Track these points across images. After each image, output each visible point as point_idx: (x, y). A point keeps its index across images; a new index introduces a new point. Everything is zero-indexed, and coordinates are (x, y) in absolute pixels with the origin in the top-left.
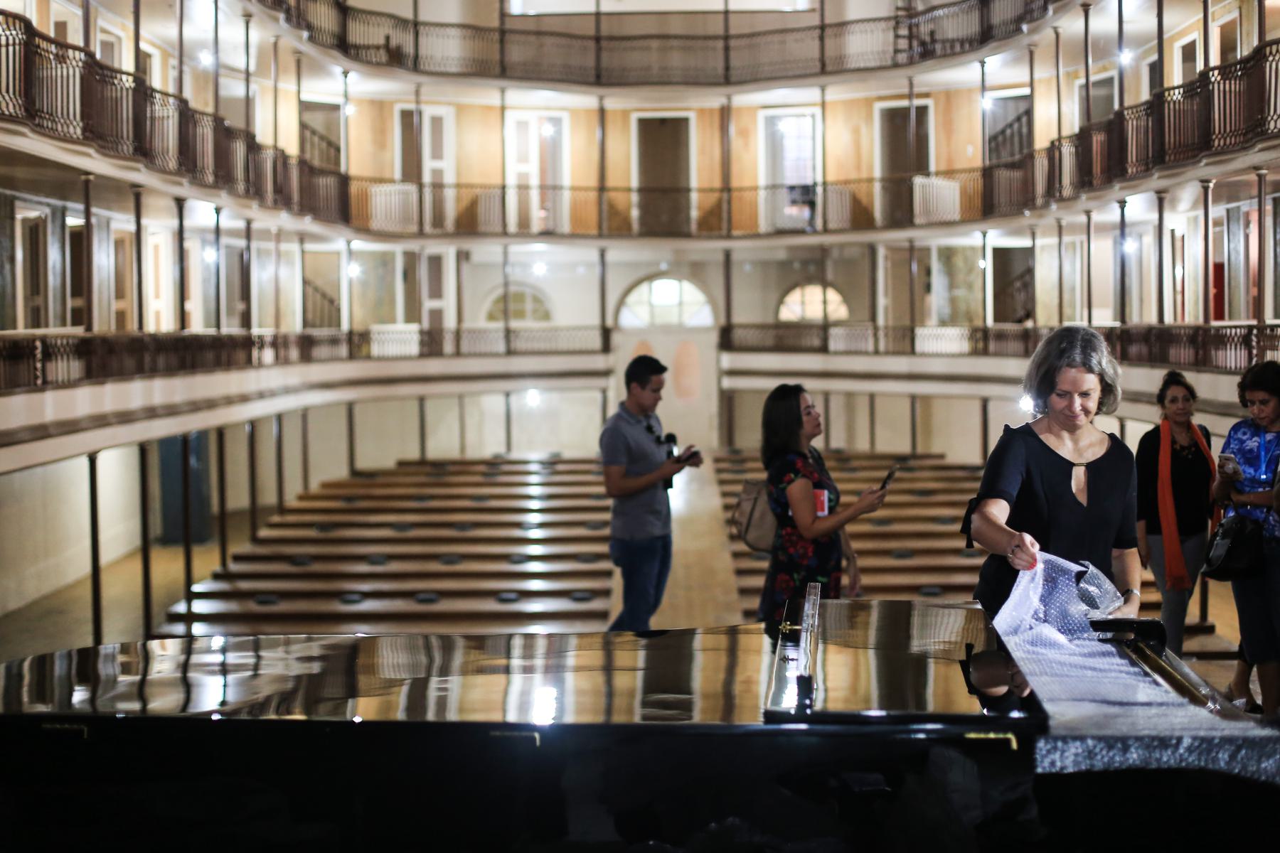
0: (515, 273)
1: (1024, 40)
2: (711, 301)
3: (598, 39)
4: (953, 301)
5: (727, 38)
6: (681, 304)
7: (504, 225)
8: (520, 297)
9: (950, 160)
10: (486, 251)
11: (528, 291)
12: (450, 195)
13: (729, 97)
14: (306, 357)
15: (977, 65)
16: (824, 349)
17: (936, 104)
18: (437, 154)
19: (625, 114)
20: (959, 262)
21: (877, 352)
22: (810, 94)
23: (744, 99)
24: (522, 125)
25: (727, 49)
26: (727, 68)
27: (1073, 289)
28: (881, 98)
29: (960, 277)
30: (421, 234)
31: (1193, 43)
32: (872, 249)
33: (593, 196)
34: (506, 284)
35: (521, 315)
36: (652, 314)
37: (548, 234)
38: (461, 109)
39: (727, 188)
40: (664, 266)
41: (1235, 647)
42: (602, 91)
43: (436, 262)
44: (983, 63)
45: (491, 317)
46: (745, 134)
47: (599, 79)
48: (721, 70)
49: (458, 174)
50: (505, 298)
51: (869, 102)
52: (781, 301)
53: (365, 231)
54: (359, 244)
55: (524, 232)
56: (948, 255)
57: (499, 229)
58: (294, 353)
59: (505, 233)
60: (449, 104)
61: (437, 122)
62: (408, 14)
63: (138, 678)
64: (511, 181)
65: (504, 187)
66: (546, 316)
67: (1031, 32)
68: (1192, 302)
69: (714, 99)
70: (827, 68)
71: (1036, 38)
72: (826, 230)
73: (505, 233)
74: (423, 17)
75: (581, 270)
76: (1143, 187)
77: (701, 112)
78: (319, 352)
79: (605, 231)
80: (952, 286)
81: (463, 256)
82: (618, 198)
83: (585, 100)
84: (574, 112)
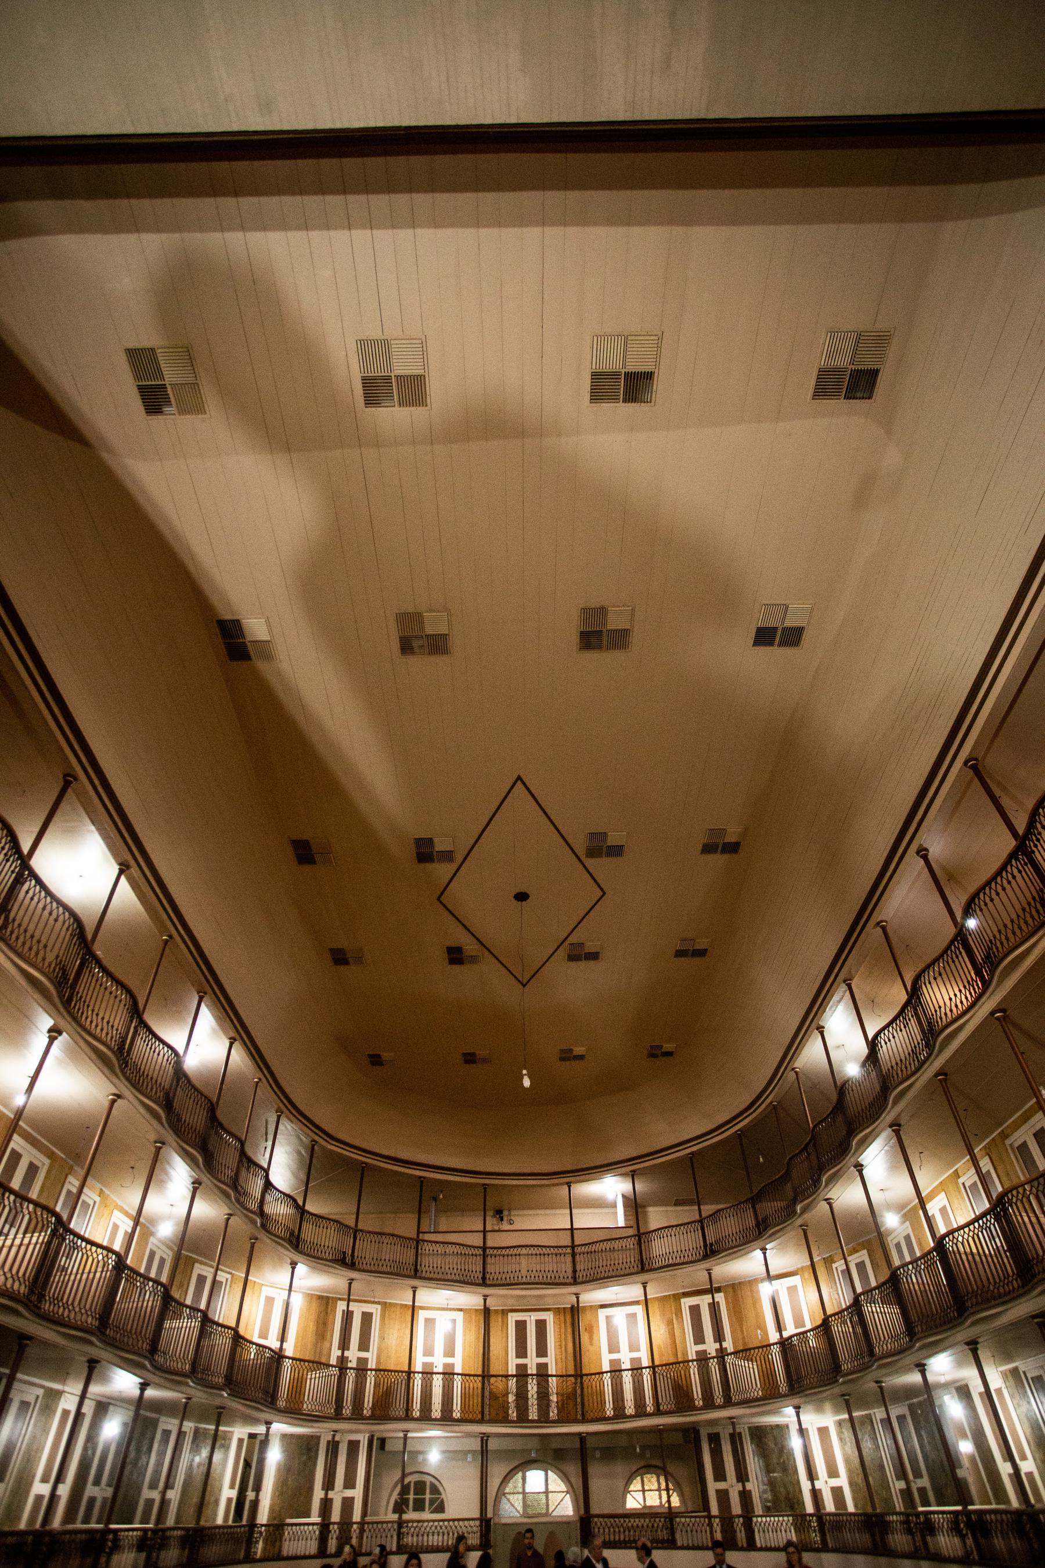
2: (572, 1490)
5: (572, 1229)
6: (547, 1492)
8: (420, 1487)
9: (745, 1343)
11: (428, 1479)
12: (370, 1379)
13: (577, 1295)
15: (758, 1253)
17: (726, 1298)
22: (631, 1291)
24: (430, 1322)
26: (575, 1271)
27: (882, 1467)
30: (338, 1416)
33: (477, 1383)
36: (525, 1506)
37: (447, 1418)
38: (385, 1305)
39: (579, 1375)
41: (542, 1473)
44: (764, 1250)
48: (570, 1274)
49: (378, 1362)
51: (677, 1297)
52: (626, 1491)
53: (294, 1412)
54: (279, 1427)
55: (426, 1417)
56: (759, 1434)
57: (402, 1414)
60: (378, 1303)
61: (367, 1318)
62: (352, 1224)
63: (1034, 1100)
64: (418, 1367)
65: (410, 1373)
66: (441, 1508)
67: (804, 1210)
69: (565, 1296)
70: (643, 1266)
71: (807, 1216)
72: (658, 1412)
76: (951, 1340)
79: (487, 1417)
80: (768, 1469)
82: (497, 1384)
83: (469, 1299)
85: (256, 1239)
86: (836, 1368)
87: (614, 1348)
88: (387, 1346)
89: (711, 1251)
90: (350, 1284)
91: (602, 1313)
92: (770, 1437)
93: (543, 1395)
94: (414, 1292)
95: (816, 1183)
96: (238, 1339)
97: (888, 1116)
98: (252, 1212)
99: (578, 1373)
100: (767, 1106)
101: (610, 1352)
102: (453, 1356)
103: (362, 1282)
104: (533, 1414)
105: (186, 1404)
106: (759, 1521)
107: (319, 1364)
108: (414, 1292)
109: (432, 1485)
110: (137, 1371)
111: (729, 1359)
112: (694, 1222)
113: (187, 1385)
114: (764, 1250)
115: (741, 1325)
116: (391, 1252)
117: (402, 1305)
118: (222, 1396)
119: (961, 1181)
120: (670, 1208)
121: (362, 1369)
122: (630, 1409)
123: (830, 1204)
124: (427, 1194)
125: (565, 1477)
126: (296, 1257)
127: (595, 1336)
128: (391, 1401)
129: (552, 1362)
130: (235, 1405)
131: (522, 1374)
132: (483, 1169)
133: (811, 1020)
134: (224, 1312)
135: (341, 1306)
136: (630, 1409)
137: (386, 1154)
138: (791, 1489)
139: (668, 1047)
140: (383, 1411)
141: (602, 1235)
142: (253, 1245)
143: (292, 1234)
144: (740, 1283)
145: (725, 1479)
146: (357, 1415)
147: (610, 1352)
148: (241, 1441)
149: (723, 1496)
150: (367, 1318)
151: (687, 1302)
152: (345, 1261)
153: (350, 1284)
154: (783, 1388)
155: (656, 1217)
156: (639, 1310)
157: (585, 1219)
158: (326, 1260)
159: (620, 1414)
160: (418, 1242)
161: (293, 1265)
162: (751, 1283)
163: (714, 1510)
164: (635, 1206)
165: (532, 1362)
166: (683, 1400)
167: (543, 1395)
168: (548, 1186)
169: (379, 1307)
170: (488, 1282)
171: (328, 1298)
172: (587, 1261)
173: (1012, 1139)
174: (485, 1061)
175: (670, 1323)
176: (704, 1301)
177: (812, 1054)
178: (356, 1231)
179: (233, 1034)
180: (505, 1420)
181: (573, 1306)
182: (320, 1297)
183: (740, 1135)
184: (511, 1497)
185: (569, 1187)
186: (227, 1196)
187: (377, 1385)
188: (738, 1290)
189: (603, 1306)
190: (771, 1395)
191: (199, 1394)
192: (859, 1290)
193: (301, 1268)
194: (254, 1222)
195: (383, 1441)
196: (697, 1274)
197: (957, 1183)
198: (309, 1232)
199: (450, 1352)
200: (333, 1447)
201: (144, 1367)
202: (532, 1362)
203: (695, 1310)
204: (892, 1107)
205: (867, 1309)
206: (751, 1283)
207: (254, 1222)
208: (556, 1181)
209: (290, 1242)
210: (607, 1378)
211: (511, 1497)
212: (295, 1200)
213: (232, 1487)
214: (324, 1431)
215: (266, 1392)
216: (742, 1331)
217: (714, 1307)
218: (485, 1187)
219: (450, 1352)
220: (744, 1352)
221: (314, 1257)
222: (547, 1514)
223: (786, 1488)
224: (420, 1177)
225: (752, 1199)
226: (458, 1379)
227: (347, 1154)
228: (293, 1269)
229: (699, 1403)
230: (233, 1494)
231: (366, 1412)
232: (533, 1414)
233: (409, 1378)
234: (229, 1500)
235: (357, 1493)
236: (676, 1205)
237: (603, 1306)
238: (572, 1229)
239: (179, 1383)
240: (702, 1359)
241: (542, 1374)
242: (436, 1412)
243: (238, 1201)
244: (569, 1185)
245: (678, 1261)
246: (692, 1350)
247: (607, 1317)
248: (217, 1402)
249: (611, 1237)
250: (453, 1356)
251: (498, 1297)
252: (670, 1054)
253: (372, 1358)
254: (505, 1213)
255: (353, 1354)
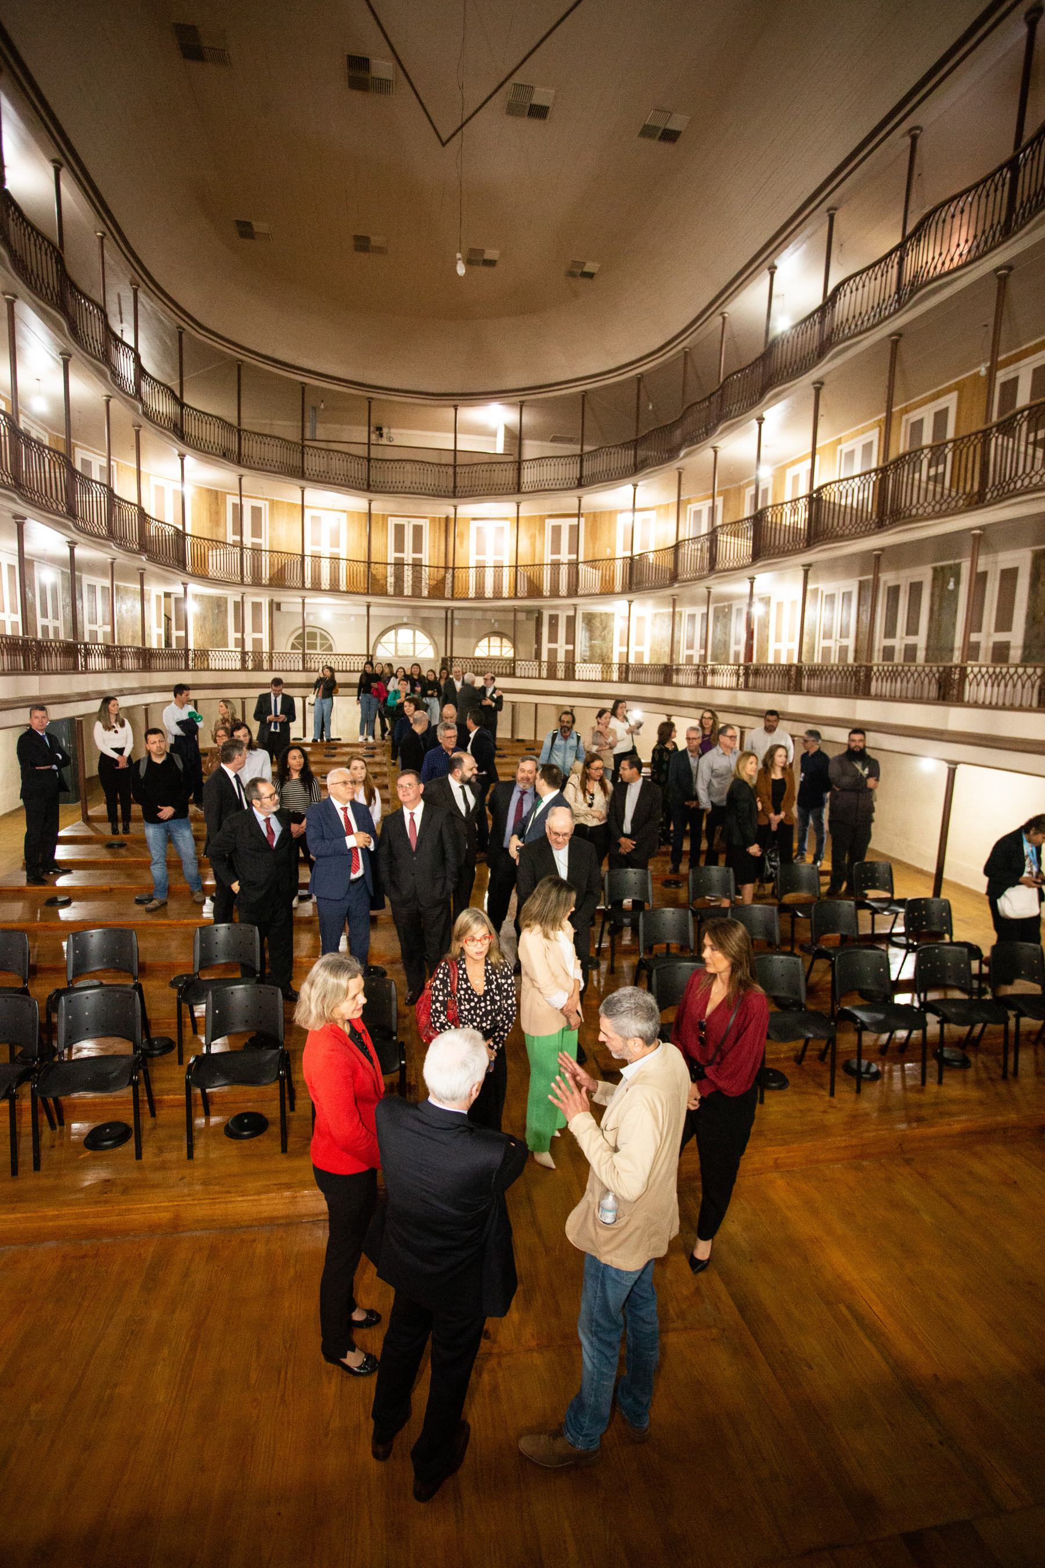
0: (310, 621)
1: (676, 464)
3: (369, 460)
4: (592, 647)
5: (455, 451)
7: (303, 582)
8: (313, 636)
10: (291, 601)
11: (318, 631)
12: (265, 558)
14: (147, 668)
16: (512, 675)
18: (257, 532)
19: (385, 518)
20: (597, 623)
21: (540, 678)
22: (505, 508)
23: (468, 509)
24: (315, 519)
25: (455, 473)
26: (455, 487)
28: (551, 516)
29: (597, 633)
31: (946, 410)
32: (540, 614)
33: (362, 568)
34: (304, 627)
35: (313, 646)
37: (334, 589)
38: (273, 504)
40: (405, 620)
42: (372, 496)
43: (256, 606)
44: (635, 486)
45: (293, 647)
46: (462, 536)
47: (368, 487)
49: (271, 544)
50: (301, 637)
51: (542, 519)
52: (476, 645)
53: (202, 577)
54: (195, 588)
55: (316, 588)
56: (589, 619)
57: (299, 585)
58: (130, 663)
59: (303, 588)
60: (266, 499)
61: (256, 512)
62: (235, 423)
65: (303, 556)
67: (687, 455)
68: (808, 652)
69: (444, 508)
71: (687, 460)
72: (516, 597)
73: (303, 588)
74: (244, 426)
75: (353, 619)
77: (433, 520)
78: (157, 663)
81: (275, 607)
83: (357, 502)
84: (351, 514)
85: (140, 426)
86: (674, 577)
87: (480, 551)
88: (279, 534)
89: (581, 483)
90: (240, 480)
91: (474, 525)
92: (598, 619)
93: (417, 580)
94: (303, 492)
95: (709, 432)
96: (143, 515)
97: (815, 374)
98: (130, 396)
99: (449, 567)
100: (679, 352)
101: (478, 554)
102: (338, 546)
103: (251, 480)
104: (408, 591)
105: (112, 563)
106: (578, 667)
107: (218, 543)
108: (303, 492)
109: (321, 635)
110: (64, 531)
111: (581, 566)
112: (575, 455)
113: (110, 547)
114: (635, 486)
115: (594, 543)
116: (274, 453)
117: (288, 504)
118: (142, 560)
119: (839, 448)
120: (545, 444)
121: (257, 550)
122: (489, 592)
123: (716, 452)
124: (306, 398)
125: (430, 634)
126: (185, 449)
127: (465, 541)
128: (284, 577)
129: (425, 557)
130: (150, 567)
131: (399, 564)
132: (379, 384)
133: (762, 259)
134: (124, 489)
135: (232, 500)
136: (489, 592)
137: (264, 353)
138: (605, 651)
139: (590, 267)
140: (279, 581)
141: (486, 459)
142: (137, 432)
143: (175, 425)
144: (601, 513)
145: (556, 642)
146: (257, 582)
147: (478, 554)
148: (158, 597)
149: (553, 653)
150: (256, 512)
151: (550, 523)
152: (233, 455)
153: (240, 480)
154: (618, 588)
155: (531, 449)
156: (508, 527)
157: (466, 443)
158: (214, 455)
159: (480, 596)
160: (303, 447)
161: (182, 457)
162: (612, 514)
163: (545, 657)
164: (516, 438)
165: (408, 556)
166: (535, 591)
167: (417, 580)
168: (422, 405)
169: (267, 503)
170: (372, 488)
171: (217, 492)
172: (461, 478)
173: (910, 415)
174: (380, 250)
175: (533, 537)
176: (566, 523)
177: (751, 301)
178: (239, 431)
179: (57, 156)
180: (385, 594)
181: (447, 519)
182: (209, 490)
183: (639, 379)
184: (386, 645)
185: (456, 410)
186: (102, 374)
187: (271, 565)
188: (597, 519)
189: (474, 519)
190: (607, 592)
191: (121, 556)
192: (719, 522)
193: (189, 460)
194: (136, 410)
195: (279, 605)
196: (568, 501)
197: (835, 450)
198: (192, 427)
199: (336, 543)
200: (239, 606)
201: (68, 528)
202: (408, 556)
203: (557, 530)
204: (829, 361)
205: (721, 538)
206: (612, 514)
207: (136, 410)
208: (428, 402)
209: (174, 432)
210: (472, 573)
211: (386, 645)
212: (172, 392)
213: (159, 626)
214: (232, 595)
215: (178, 561)
216: (594, 548)
217: (575, 530)
218: (370, 400)
219: (336, 543)
220: (593, 562)
221: (205, 452)
222: (414, 656)
223: (601, 649)
224: (302, 383)
225: (636, 441)
226: (343, 564)
227: (220, 347)
228: (182, 460)
229: (547, 593)
230: (162, 631)
231: (265, 581)
232: (408, 591)
233: (369, 567)
234: (159, 636)
235: (265, 636)
236: (551, 441)
237: (474, 519)
238: (455, 451)
239: (104, 545)
240: (556, 565)
241: (417, 565)
242: (325, 584)
243: (115, 383)
244: (456, 408)
245: (553, 487)
246: (548, 558)
247: (478, 528)
248: (138, 564)
249: (491, 462)
250: (338, 546)
251: (381, 505)
252: (590, 275)
253: (265, 543)
254: (385, 430)
255: (248, 540)
